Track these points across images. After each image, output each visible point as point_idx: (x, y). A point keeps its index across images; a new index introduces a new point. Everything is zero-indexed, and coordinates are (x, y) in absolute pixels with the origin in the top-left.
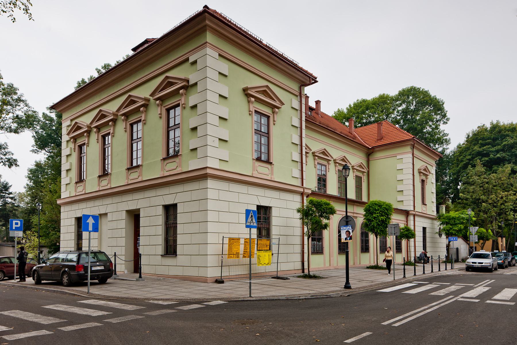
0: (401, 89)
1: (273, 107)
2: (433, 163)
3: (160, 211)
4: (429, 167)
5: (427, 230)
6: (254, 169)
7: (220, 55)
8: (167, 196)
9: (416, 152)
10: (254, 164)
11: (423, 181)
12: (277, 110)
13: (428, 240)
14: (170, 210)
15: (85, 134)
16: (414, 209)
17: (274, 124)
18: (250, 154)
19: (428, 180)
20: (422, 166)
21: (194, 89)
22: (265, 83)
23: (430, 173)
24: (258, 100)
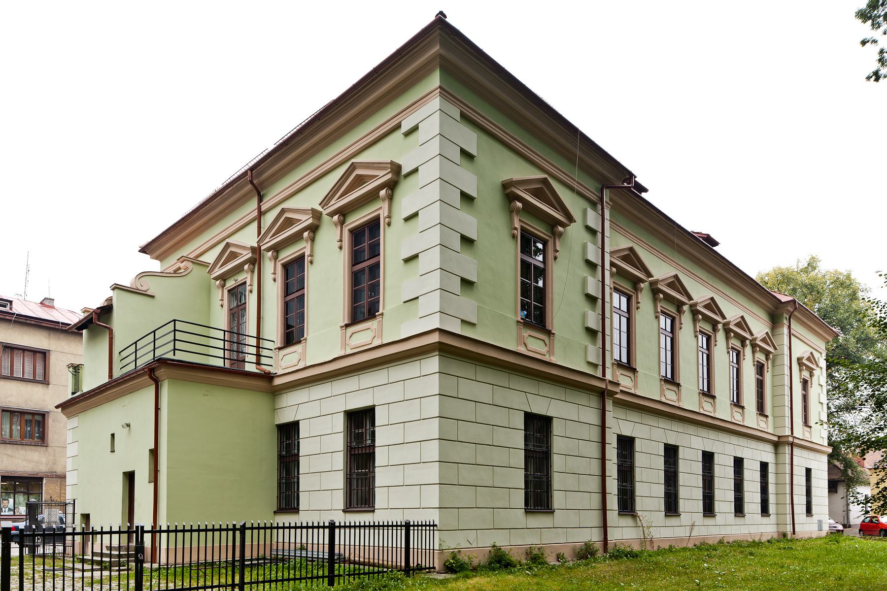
0: (829, 266)
1: (552, 224)
2: (822, 346)
3: (339, 423)
4: (815, 353)
5: (771, 468)
6: (662, 393)
7: (463, 116)
8: (355, 394)
9: (795, 326)
10: (661, 385)
11: (805, 383)
12: (560, 229)
13: (771, 488)
14: (360, 422)
15: (246, 267)
16: (792, 433)
17: (555, 258)
18: (513, 313)
19: (815, 379)
20: (805, 352)
21: (412, 179)
22: (546, 176)
23: (818, 366)
24: (529, 209)
